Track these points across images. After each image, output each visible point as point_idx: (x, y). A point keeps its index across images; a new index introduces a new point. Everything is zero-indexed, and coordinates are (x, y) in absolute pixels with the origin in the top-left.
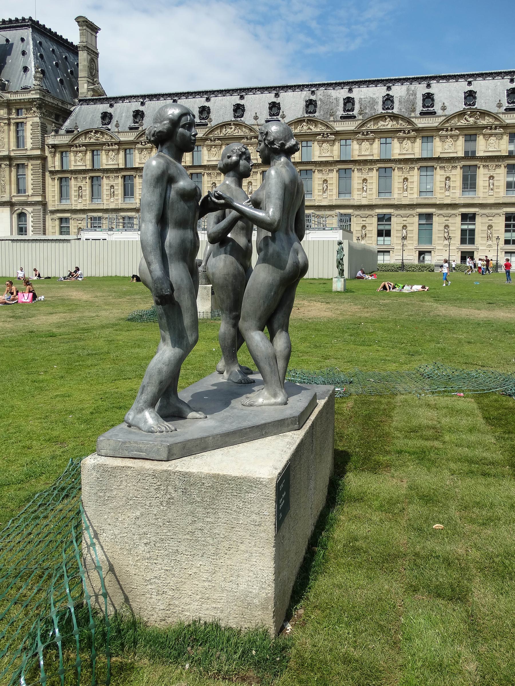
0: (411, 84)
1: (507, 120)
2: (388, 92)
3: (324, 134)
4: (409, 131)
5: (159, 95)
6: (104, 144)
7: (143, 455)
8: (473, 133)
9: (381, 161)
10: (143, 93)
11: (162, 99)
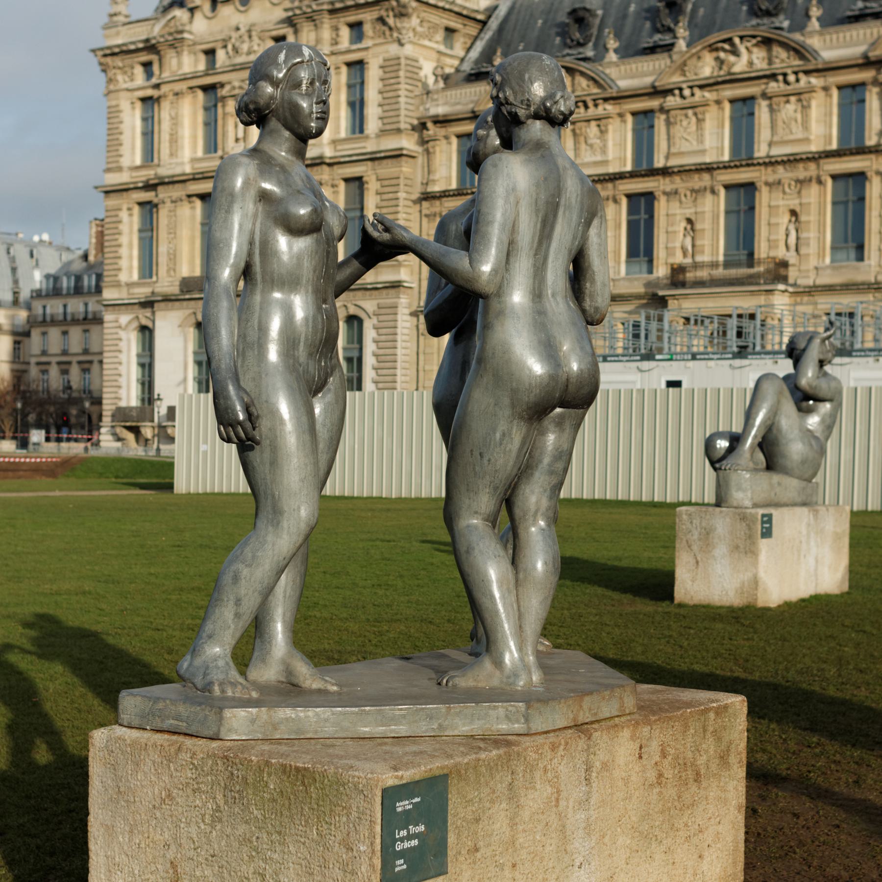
7: (183, 726)
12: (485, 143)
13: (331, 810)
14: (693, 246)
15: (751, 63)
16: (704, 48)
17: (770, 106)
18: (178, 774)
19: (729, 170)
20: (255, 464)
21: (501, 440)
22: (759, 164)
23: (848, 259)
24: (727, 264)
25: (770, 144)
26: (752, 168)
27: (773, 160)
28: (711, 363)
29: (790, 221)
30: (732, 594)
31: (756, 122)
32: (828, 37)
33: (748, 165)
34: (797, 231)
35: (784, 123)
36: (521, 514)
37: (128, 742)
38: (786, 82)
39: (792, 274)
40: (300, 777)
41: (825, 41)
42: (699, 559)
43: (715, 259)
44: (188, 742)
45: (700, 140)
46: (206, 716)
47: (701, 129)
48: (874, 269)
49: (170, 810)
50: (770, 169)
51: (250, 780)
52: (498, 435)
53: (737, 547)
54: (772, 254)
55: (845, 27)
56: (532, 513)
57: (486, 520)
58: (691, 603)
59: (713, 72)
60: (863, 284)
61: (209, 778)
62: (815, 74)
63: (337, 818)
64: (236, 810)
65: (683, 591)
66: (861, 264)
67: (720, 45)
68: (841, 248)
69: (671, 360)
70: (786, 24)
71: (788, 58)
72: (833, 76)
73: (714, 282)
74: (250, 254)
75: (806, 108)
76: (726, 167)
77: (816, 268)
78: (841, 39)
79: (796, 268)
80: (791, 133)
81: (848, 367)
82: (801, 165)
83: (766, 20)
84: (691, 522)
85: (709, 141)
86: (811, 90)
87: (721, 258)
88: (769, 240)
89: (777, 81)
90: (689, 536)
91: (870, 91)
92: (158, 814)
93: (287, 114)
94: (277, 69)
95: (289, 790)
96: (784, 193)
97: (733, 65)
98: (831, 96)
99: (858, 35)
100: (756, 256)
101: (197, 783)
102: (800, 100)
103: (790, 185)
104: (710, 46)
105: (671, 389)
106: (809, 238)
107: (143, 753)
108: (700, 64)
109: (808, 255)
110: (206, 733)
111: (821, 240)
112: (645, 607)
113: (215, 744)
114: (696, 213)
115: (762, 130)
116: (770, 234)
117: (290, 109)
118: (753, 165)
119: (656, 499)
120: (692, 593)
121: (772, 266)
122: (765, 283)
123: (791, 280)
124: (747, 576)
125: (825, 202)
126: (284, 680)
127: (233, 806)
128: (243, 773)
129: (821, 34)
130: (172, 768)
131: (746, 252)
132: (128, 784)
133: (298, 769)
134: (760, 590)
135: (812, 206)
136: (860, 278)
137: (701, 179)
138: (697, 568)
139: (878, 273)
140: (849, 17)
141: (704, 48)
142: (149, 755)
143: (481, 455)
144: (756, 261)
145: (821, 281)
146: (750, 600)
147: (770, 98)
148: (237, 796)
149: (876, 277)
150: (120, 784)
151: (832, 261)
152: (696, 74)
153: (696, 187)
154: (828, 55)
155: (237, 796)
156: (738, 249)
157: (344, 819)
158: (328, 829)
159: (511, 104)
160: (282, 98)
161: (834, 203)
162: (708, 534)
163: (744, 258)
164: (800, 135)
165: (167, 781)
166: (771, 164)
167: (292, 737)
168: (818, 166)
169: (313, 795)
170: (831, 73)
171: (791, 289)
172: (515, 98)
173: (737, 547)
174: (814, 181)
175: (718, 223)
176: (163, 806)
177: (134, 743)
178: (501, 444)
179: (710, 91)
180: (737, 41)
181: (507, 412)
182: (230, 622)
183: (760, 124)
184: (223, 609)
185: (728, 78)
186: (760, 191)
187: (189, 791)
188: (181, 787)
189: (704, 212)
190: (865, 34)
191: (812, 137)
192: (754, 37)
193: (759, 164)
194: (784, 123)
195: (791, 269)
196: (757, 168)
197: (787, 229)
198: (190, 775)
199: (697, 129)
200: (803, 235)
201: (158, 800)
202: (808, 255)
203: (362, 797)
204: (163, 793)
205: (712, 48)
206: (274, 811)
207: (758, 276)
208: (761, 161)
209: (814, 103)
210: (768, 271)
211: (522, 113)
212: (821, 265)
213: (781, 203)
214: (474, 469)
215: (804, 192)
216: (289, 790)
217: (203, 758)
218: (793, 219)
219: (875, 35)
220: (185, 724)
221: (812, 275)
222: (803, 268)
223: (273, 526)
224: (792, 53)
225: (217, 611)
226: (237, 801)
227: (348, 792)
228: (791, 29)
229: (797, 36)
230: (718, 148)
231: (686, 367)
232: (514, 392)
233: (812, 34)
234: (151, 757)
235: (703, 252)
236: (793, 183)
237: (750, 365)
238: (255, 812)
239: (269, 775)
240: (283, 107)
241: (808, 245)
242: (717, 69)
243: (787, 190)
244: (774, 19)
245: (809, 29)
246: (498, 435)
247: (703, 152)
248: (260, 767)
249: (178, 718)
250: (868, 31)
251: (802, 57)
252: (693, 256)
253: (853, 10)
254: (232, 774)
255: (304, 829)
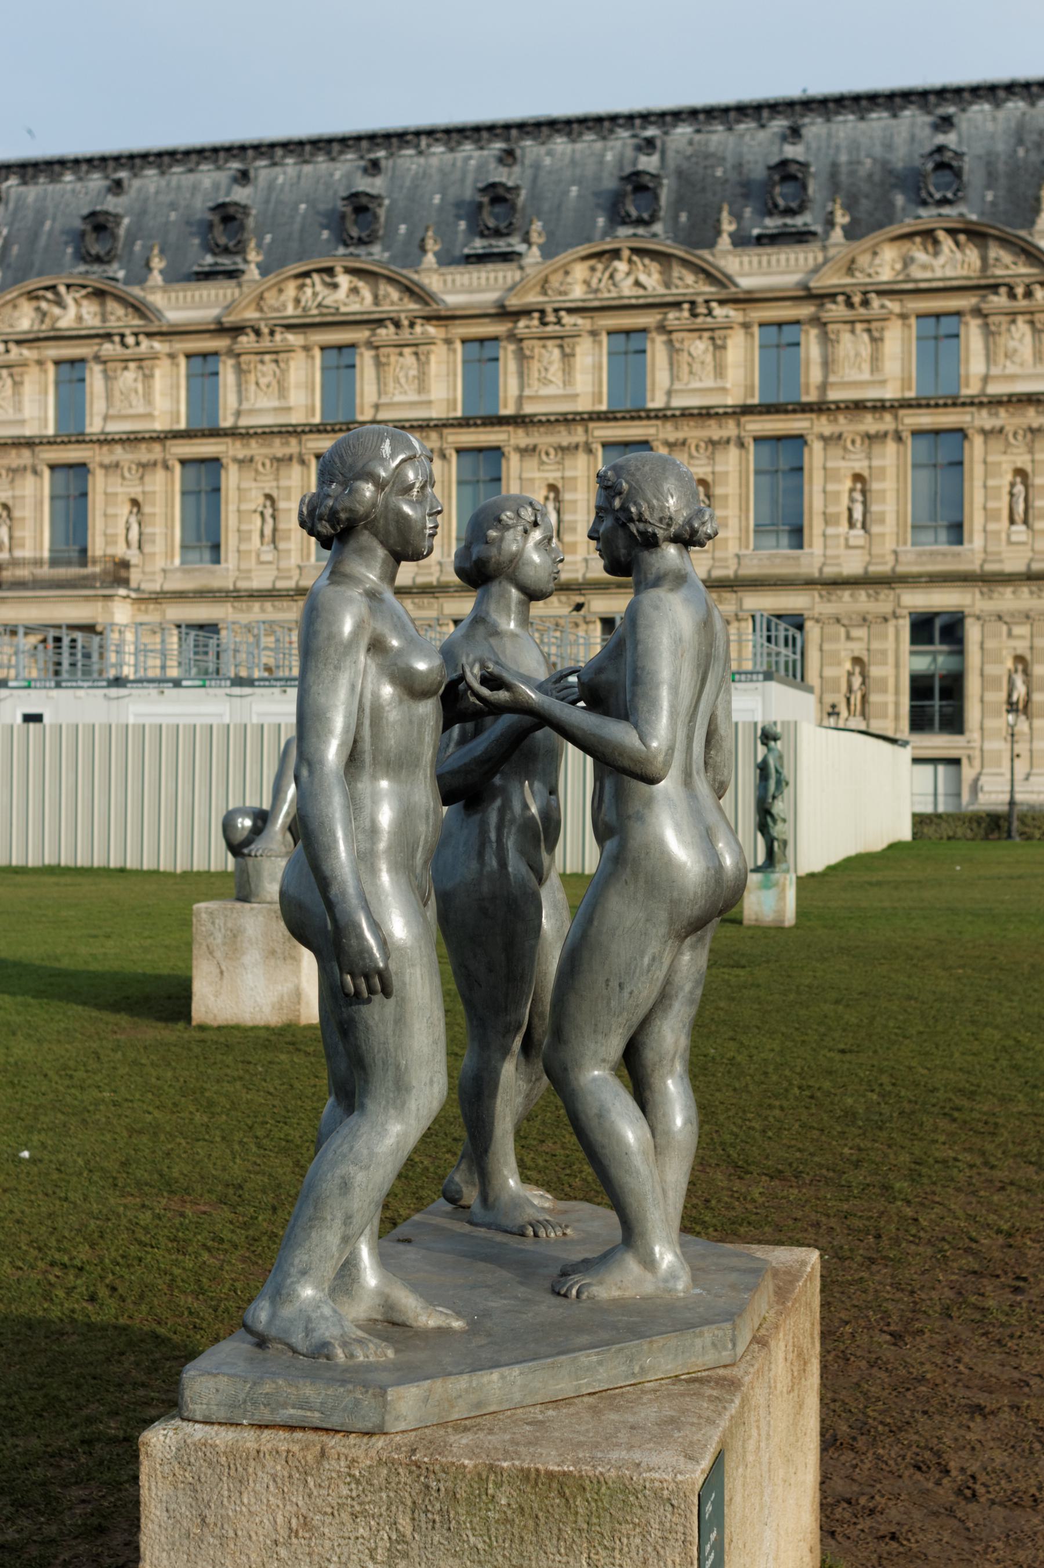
0: (135, 175)
1: (743, 275)
2: (940, 139)
3: (693, 303)
4: (1028, 286)
5: (62, 163)
6: (832, 297)
7: (315, 1417)
8: (471, 336)
9: (919, 406)
10: (792, 91)
11: (69, 177)
12: (500, 548)
13: (613, 1530)
14: (11, 538)
15: (79, 318)
16: (21, 295)
17: (105, 372)
18: (324, 1492)
19: (55, 447)
20: (371, 1022)
21: (650, 966)
22: (91, 441)
23: (201, 561)
24: (54, 562)
25: (106, 418)
26: (83, 446)
27: (109, 437)
28: (81, 693)
29: (131, 512)
30: (267, 1010)
31: (88, 390)
32: (173, 295)
33: (78, 442)
34: (140, 524)
35: (122, 393)
36: (657, 1058)
37: (222, 1448)
38: (124, 345)
39: (135, 576)
40: (555, 1485)
41: (169, 299)
42: (224, 968)
43: (38, 555)
44: (333, 1442)
45: (18, 407)
46: (357, 1402)
47: (19, 394)
48: (233, 574)
49: (309, 1546)
50: (105, 448)
51: (461, 1494)
52: (646, 960)
53: (273, 952)
54: (110, 551)
55: (193, 285)
56: (669, 1057)
57: (612, 1069)
58: (215, 1024)
59: (32, 326)
60: (220, 591)
61: (384, 1495)
62: (159, 338)
63: (625, 1541)
64: (436, 1539)
65: (203, 1009)
66: (217, 567)
67: (41, 293)
68: (194, 548)
69: (29, 687)
70: (121, 274)
71: (126, 315)
72: (181, 341)
73: (37, 584)
74: (359, 725)
75: (148, 377)
76: (51, 442)
77: (164, 571)
78: (189, 299)
79: (139, 570)
80: (131, 406)
81: (249, 699)
82: (143, 446)
83: (96, 268)
84: (213, 923)
85: (29, 410)
86: (155, 357)
87: (46, 554)
88: (105, 535)
89: (113, 342)
90: (210, 940)
91: (225, 363)
92: (283, 1552)
93: (392, 528)
94: (382, 465)
95: (536, 1505)
96: (123, 478)
97: (58, 319)
98: (178, 365)
99: (209, 295)
100: (90, 553)
101: (360, 1504)
102: (140, 368)
103: (130, 469)
104: (29, 293)
105: (32, 725)
106: (154, 534)
107: (252, 1463)
108: (16, 314)
109: (154, 554)
110: (360, 1426)
111: (169, 537)
112: (154, 1032)
113: (380, 1442)
114: (14, 497)
115: (95, 401)
116: (106, 527)
117: (397, 522)
118: (84, 442)
119: (14, 863)
120: (216, 1011)
121: (110, 566)
122: (102, 587)
123: (133, 584)
124: (285, 988)
125: (173, 491)
126: (379, 1317)
127: (431, 1533)
128: (449, 1484)
129: (165, 290)
130: (311, 1484)
131: (77, 548)
132: (223, 1512)
133: (550, 1475)
134: (303, 1004)
135: (158, 496)
136: (216, 583)
137: (19, 456)
138: (221, 979)
139: (237, 578)
140: (197, 273)
141: (21, 295)
142: (264, 1466)
143: (621, 986)
144: (90, 559)
145: (169, 586)
146: (291, 1017)
147: (105, 362)
148: (437, 1518)
149: (235, 584)
150: (207, 1512)
151: (183, 563)
152: (11, 326)
153: (14, 465)
154: (174, 316)
155: (437, 1518)
156: (67, 544)
157: (638, 1541)
158: (609, 1556)
159: (646, 521)
160: (386, 506)
161: (184, 493)
162: (235, 936)
163: (75, 555)
164: (141, 410)
165: (300, 1503)
166: (106, 442)
167: (473, 1414)
168: (164, 446)
169: (580, 1510)
170: (178, 337)
171: (133, 595)
172: (651, 514)
173: (273, 952)
174: (159, 466)
175: (42, 511)
176: (294, 1540)
177: (232, 1452)
178: (649, 971)
179: (29, 348)
180: (62, 289)
181: (663, 930)
182: (334, 1249)
183: (92, 393)
184: (324, 1232)
185: (52, 334)
186: (94, 475)
187: (345, 1516)
188: (329, 1510)
189: (23, 497)
190: (217, 296)
191: (156, 413)
192: (84, 287)
193: (91, 441)
194: (122, 393)
195: (132, 570)
196: (90, 446)
197: (127, 522)
198: (345, 1492)
199: (14, 394)
200: (147, 530)
201: (284, 1532)
202: (154, 554)
203: (669, 1508)
204: (294, 1521)
205: (32, 296)
206: (509, 1536)
207: (93, 577)
208: (95, 438)
209: (157, 373)
210: (105, 572)
211: (660, 533)
212: (169, 567)
213: (120, 490)
214: (608, 1003)
215: (147, 479)
216: (536, 1505)
217: (370, 1467)
218: (135, 510)
219: (229, 298)
220: (317, 1415)
221: (159, 577)
222: (147, 569)
223: (396, 1108)
224: (130, 310)
225: (313, 1234)
226: (438, 1525)
227: (643, 1502)
228: (127, 281)
229: (136, 291)
230: (39, 419)
231: (48, 697)
232: (674, 903)
233: (153, 289)
234: (268, 1469)
235: (23, 546)
236: (134, 467)
237: (130, 695)
238: (472, 1539)
239: (498, 1485)
240: (386, 518)
241: (153, 542)
242: (37, 322)
243: (127, 474)
244: (106, 267)
245: (150, 283)
246: (646, 960)
247: (22, 422)
248: (479, 1475)
249: (304, 1404)
250: (221, 292)
251: (142, 316)
252: (10, 550)
253: (200, 266)
254: (427, 1487)
255: (564, 1559)
